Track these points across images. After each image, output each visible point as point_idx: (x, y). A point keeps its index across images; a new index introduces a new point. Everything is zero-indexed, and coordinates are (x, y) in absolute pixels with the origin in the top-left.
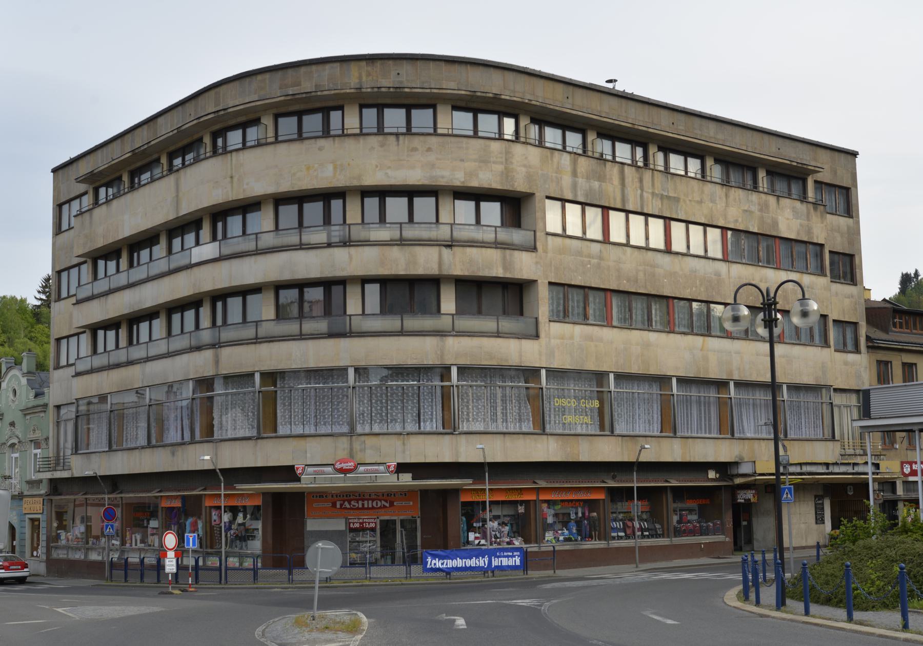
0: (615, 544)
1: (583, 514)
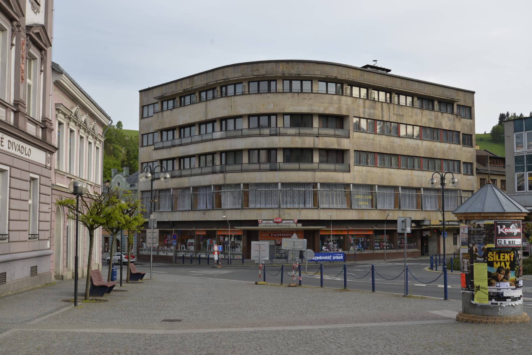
0: (376, 252)
1: (364, 240)
